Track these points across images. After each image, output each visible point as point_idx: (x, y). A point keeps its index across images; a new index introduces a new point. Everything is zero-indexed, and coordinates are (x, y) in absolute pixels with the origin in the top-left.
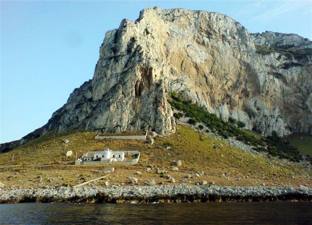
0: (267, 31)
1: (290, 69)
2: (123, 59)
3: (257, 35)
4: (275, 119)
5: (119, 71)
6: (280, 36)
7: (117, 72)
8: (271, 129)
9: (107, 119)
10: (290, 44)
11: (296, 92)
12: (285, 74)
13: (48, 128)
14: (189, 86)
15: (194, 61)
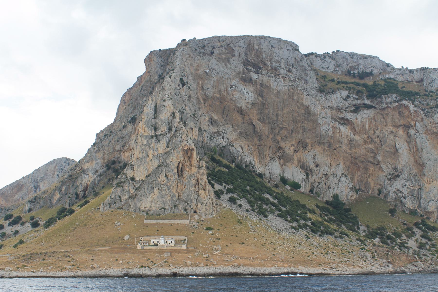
0: (338, 51)
1: (360, 113)
2: (164, 139)
3: (325, 57)
4: (338, 178)
5: (161, 151)
6: (355, 58)
7: (160, 153)
8: (331, 192)
9: (152, 202)
10: (367, 71)
11: (365, 143)
12: (353, 120)
13: (61, 191)
14: (232, 138)
15: (239, 105)
